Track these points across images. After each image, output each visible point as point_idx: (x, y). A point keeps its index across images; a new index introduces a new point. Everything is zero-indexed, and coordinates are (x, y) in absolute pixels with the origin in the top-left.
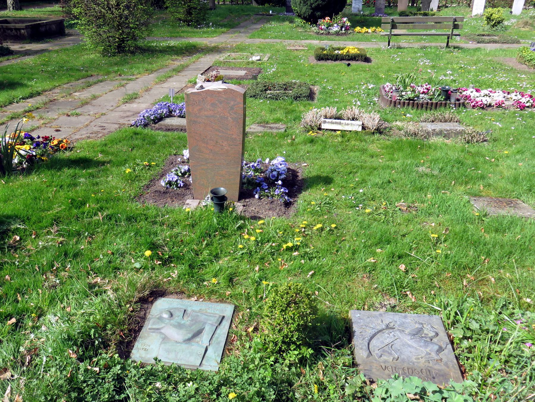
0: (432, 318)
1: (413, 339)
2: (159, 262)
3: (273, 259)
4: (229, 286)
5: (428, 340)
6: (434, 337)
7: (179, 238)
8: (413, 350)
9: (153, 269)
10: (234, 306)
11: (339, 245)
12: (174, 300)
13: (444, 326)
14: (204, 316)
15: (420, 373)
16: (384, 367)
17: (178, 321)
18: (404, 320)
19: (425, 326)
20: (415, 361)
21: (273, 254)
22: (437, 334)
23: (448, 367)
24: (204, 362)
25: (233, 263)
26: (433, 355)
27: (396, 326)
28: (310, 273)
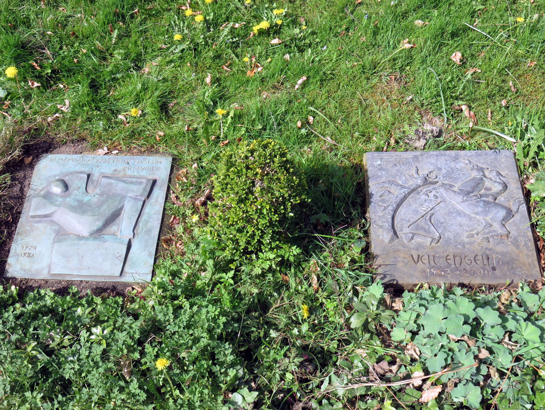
0: (499, 157)
1: (466, 201)
2: (36, 84)
3: (237, 56)
4: (161, 119)
5: (490, 199)
6: (499, 193)
7: (69, 28)
8: (464, 221)
9: (28, 97)
10: (170, 159)
11: (352, 17)
12: (69, 156)
13: (518, 167)
14: (121, 185)
15: (473, 263)
16: (415, 257)
17: (79, 197)
18: (453, 164)
19: (487, 173)
20: (466, 240)
21: (234, 46)
22: (505, 187)
23: (518, 247)
24: (126, 269)
25: (168, 72)
26: (497, 226)
27: (441, 180)
28: (300, 82)
